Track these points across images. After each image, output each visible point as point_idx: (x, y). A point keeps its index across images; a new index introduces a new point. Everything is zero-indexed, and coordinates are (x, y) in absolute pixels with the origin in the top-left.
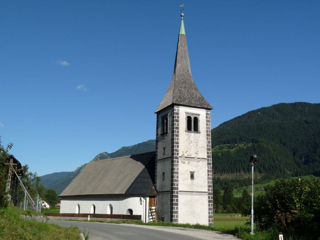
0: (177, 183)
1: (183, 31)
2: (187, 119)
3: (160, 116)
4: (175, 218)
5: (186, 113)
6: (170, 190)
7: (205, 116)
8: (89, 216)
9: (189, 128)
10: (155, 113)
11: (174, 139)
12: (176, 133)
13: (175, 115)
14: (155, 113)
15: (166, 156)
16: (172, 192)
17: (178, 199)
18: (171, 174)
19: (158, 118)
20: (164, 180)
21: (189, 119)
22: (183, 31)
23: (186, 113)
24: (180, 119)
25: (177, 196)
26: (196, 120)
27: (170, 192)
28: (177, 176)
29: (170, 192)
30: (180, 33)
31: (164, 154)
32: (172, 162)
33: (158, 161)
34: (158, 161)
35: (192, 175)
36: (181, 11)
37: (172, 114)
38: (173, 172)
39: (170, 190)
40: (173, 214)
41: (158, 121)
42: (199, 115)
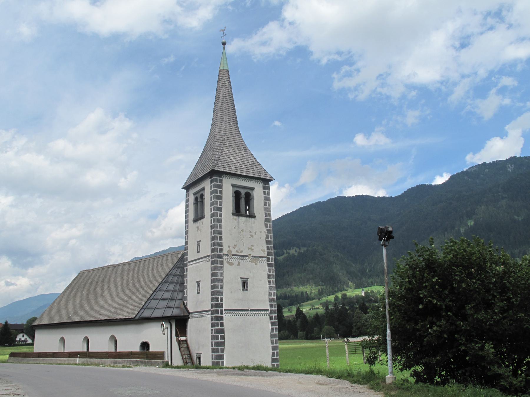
2: (234, 195)
9: (237, 212)
19: (187, 195)
20: (199, 293)
21: (237, 195)
23: (233, 186)
26: (249, 198)
27: (210, 257)
29: (210, 257)
34: (189, 264)
35: (244, 283)
42: (253, 189)
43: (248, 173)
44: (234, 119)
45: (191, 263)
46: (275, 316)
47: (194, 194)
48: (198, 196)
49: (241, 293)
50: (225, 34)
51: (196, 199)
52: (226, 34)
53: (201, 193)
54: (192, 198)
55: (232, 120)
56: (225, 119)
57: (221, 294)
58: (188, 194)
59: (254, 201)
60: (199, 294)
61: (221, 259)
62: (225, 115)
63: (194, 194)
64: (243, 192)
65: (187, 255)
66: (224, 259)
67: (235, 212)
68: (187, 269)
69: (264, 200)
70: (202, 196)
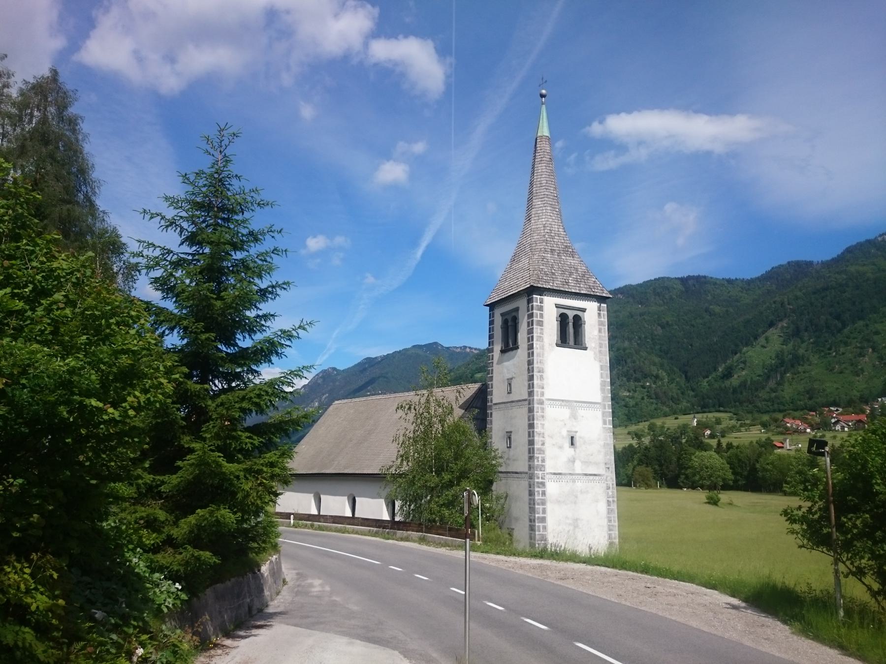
0: (543, 455)
1: (544, 130)
2: (559, 319)
3: (498, 312)
4: (541, 515)
5: (558, 306)
6: (526, 396)
7: (596, 311)
8: (292, 516)
9: (563, 341)
10: (487, 305)
11: (534, 315)
12: (537, 302)
13: (534, 311)
14: (487, 305)
15: (514, 397)
16: (531, 477)
17: (545, 491)
18: (527, 435)
19: (491, 316)
20: (510, 447)
21: (563, 319)
22: (544, 130)
23: (558, 306)
24: (546, 320)
25: (543, 484)
26: (578, 322)
27: (527, 403)
28: (542, 441)
29: (527, 403)
30: (539, 134)
31: (509, 393)
32: (531, 410)
33: (494, 407)
34: (494, 407)
35: (572, 438)
36: (540, 86)
37: (530, 308)
38: (533, 432)
39: (526, 396)
40: (536, 472)
41: (491, 323)
42: (584, 310)
43: (578, 288)
44: (557, 210)
45: (497, 407)
46: (609, 420)
47: (502, 315)
48: (509, 318)
49: (569, 451)
50: (544, 81)
51: (505, 323)
52: (546, 81)
53: (514, 314)
54: (498, 321)
55: (554, 212)
56: (544, 211)
57: (542, 452)
58: (493, 314)
59: (584, 327)
60: (511, 395)
61: (543, 524)
62: (546, 205)
63: (502, 315)
64: (571, 314)
65: (492, 395)
66: (547, 406)
67: (559, 342)
68: (491, 413)
69: (599, 325)
70: (515, 320)
